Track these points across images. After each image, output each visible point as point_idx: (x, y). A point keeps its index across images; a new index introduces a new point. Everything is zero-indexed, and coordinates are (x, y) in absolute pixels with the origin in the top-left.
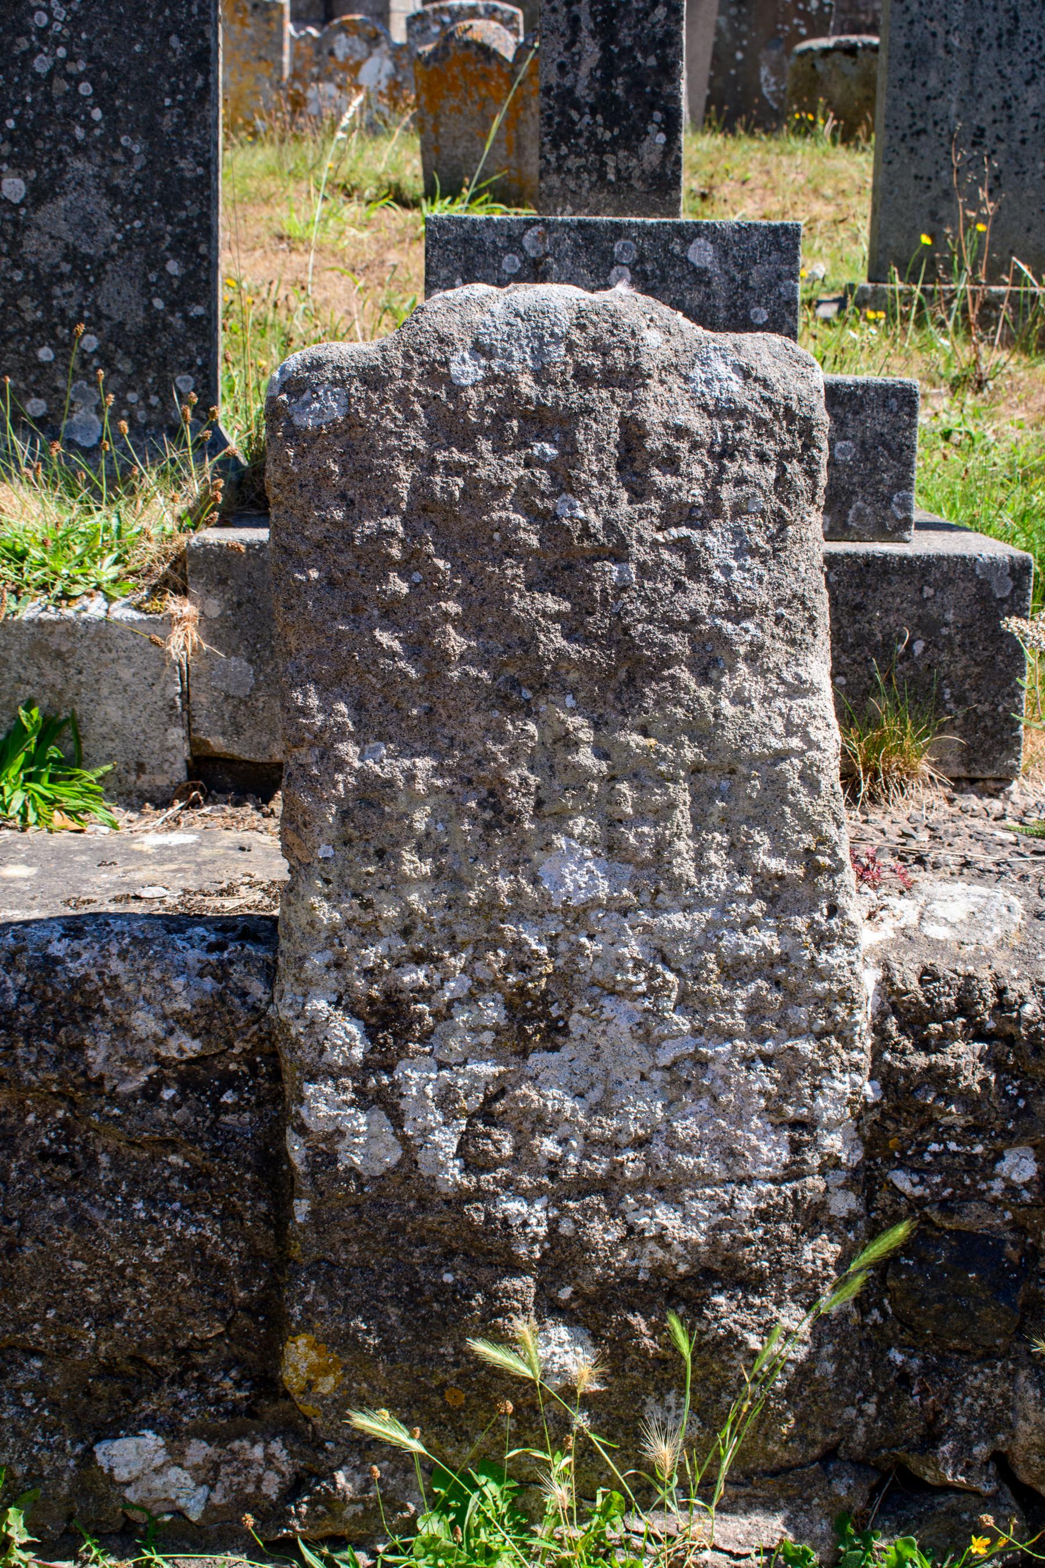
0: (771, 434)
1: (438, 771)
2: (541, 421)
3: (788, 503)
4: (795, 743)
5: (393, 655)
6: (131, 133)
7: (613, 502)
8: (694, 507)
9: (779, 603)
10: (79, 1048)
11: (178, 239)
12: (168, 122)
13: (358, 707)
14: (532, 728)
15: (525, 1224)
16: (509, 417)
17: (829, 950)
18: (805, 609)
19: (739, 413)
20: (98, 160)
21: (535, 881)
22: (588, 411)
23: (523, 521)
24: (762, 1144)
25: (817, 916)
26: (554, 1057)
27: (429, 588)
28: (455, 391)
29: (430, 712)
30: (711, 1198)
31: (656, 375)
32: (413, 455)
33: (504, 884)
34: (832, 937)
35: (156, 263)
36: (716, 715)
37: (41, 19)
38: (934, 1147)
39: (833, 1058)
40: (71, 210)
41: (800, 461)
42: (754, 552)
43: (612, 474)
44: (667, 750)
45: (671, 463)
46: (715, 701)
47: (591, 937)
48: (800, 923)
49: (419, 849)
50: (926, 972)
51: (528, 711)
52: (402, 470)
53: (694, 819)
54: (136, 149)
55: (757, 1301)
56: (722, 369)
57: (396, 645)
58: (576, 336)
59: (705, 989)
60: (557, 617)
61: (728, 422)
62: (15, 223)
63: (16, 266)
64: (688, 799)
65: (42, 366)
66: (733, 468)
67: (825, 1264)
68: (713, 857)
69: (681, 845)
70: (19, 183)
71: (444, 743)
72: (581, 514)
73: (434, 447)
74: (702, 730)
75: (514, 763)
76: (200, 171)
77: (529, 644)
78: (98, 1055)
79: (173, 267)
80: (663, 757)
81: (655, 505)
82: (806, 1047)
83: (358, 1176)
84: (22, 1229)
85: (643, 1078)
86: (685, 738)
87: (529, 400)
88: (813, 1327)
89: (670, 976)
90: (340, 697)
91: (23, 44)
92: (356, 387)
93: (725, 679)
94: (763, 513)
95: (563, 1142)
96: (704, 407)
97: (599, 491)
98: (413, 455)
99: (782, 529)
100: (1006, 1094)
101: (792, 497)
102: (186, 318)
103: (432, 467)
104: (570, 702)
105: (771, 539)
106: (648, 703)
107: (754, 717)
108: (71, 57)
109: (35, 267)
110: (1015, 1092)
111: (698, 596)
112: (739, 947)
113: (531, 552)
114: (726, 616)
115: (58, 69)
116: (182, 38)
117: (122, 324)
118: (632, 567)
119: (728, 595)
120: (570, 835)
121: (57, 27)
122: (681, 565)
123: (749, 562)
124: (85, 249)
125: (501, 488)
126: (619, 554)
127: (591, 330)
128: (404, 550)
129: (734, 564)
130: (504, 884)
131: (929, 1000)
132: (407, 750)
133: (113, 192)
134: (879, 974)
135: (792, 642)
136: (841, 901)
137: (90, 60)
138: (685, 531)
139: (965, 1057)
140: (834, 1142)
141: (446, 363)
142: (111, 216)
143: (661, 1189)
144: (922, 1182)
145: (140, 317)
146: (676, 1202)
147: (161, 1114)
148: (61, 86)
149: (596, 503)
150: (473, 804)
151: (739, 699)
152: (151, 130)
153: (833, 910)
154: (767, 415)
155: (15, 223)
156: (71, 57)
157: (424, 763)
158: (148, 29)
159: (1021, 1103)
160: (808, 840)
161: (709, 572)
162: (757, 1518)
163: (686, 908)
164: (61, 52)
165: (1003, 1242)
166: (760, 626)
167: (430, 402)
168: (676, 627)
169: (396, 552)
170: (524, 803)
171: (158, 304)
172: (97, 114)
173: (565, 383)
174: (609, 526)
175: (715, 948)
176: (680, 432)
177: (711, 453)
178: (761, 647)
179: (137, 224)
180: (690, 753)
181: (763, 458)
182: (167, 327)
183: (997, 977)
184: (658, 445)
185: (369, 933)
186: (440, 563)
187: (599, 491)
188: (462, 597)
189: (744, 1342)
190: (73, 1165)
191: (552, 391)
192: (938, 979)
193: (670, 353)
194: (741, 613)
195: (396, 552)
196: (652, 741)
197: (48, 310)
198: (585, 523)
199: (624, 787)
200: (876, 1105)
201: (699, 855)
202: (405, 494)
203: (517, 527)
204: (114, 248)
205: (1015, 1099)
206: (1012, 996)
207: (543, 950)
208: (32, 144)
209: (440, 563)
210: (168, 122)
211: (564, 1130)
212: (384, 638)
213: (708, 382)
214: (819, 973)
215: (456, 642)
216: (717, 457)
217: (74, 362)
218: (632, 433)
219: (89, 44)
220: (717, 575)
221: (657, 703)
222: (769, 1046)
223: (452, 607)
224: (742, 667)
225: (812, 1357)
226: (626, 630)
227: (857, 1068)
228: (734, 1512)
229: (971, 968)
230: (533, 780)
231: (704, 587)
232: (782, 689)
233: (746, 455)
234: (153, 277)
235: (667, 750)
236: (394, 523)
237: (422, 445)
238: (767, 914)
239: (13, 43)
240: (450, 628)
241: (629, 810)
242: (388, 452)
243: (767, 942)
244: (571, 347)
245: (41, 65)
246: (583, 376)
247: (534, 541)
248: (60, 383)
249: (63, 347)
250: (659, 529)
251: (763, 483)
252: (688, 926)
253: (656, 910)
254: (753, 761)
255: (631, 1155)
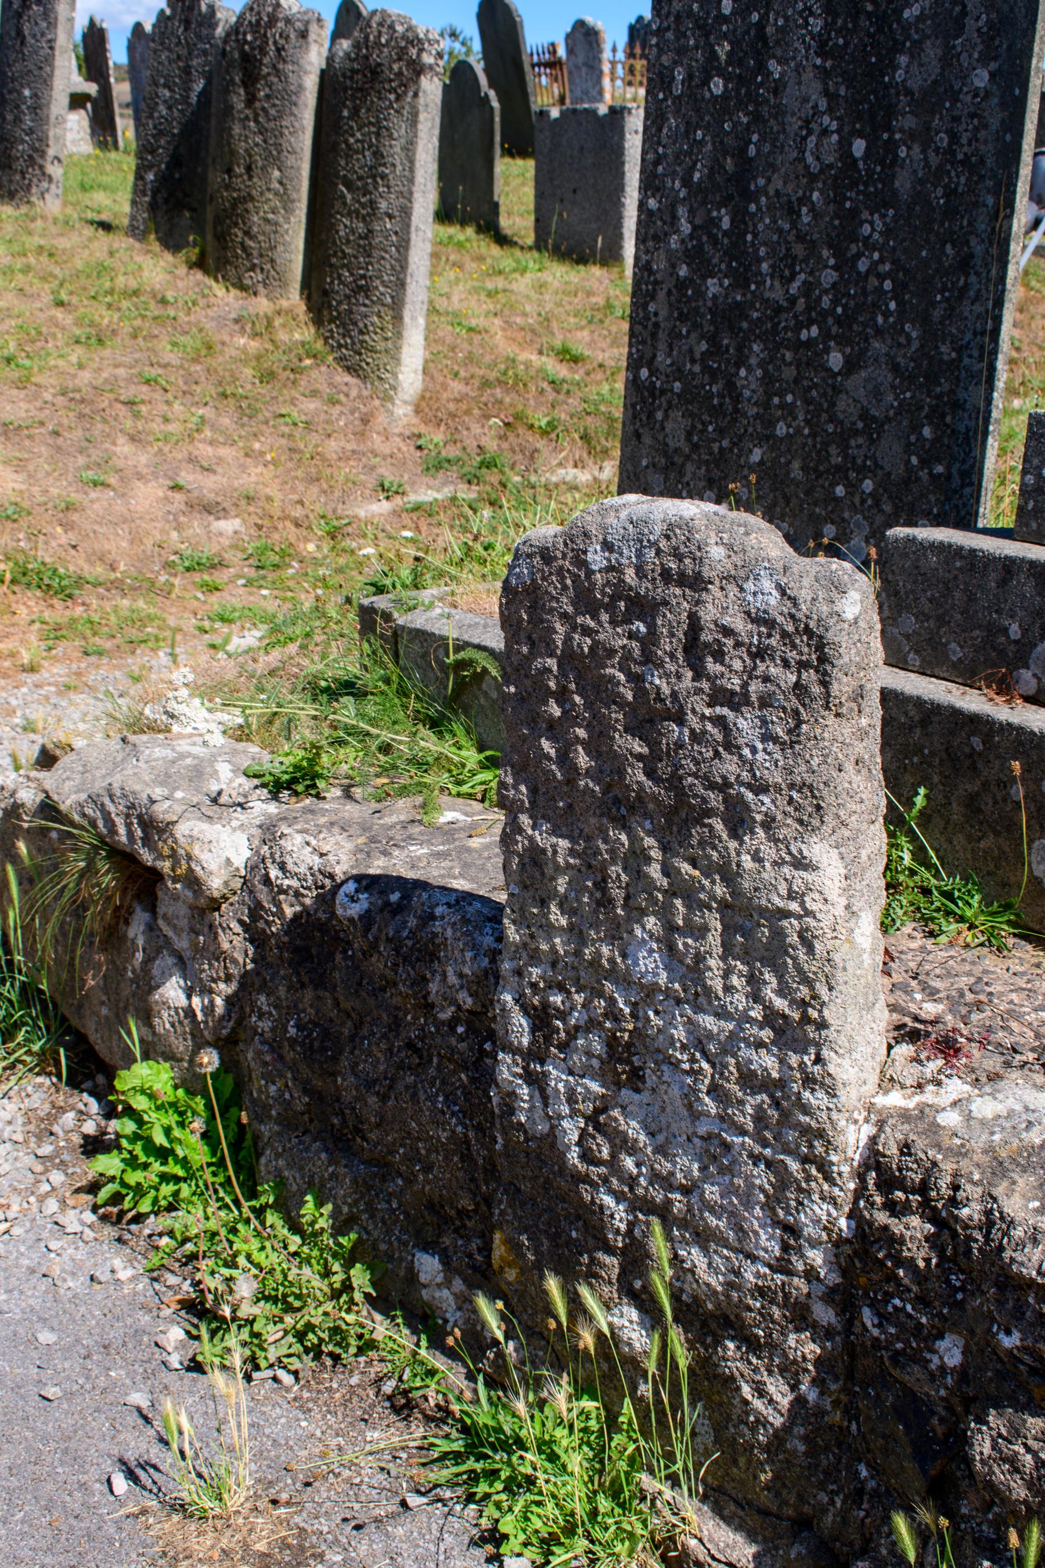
0: (794, 646)
1: (572, 852)
2: (643, 608)
3: (804, 705)
4: (794, 906)
5: (548, 757)
6: (913, 322)
7: (679, 677)
8: (733, 693)
9: (792, 786)
10: (424, 980)
11: (933, 409)
12: (937, 314)
13: (533, 791)
14: (623, 837)
15: (612, 1216)
16: (620, 599)
17: (813, 1090)
18: (814, 797)
19: (771, 624)
20: (889, 342)
21: (624, 956)
22: (665, 603)
23: (622, 677)
24: (761, 1232)
25: (806, 1058)
26: (636, 1097)
27: (569, 717)
28: (590, 573)
29: (570, 806)
30: (727, 1258)
31: (717, 582)
32: (564, 616)
33: (605, 950)
34: (815, 1081)
35: (916, 428)
36: (738, 865)
37: (866, 229)
38: (897, 1302)
39: (813, 1184)
40: (867, 380)
41: (817, 671)
42: (776, 740)
43: (680, 655)
44: (706, 883)
45: (719, 656)
46: (738, 854)
47: (657, 1013)
48: (794, 1059)
49: (560, 905)
50: (907, 1145)
51: (625, 827)
52: (558, 626)
53: (723, 945)
54: (914, 335)
55: (754, 1361)
56: (767, 585)
57: (552, 752)
58: (663, 544)
59: (727, 1085)
60: (640, 757)
61: (763, 629)
62: (834, 387)
63: (831, 420)
64: (719, 927)
65: (837, 500)
66: (761, 667)
67: (804, 1357)
68: (735, 981)
69: (712, 963)
70: (839, 355)
71: (577, 833)
72: (657, 682)
73: (578, 612)
74: (729, 875)
75: (613, 861)
76: (954, 355)
77: (621, 773)
78: (433, 987)
79: (927, 432)
80: (703, 888)
81: (705, 685)
82: (794, 1166)
83: (525, 1132)
84: (391, 1087)
85: (689, 1139)
86: (717, 877)
87: (631, 588)
88: (791, 1403)
89: (705, 1065)
90: (525, 782)
91: (854, 249)
92: (537, 560)
93: (746, 838)
94: (784, 709)
95: (638, 1165)
96: (748, 613)
97: (671, 667)
98: (564, 616)
99: (798, 726)
100: (948, 1282)
101: (807, 701)
102: (930, 474)
103: (574, 628)
104: (648, 825)
105: (790, 732)
106: (694, 842)
107: (765, 875)
108: (882, 260)
109: (842, 422)
110: (958, 1284)
111: (729, 767)
112: (751, 1062)
113: (629, 704)
114: (749, 786)
115: (872, 269)
116: (954, 246)
117: (889, 474)
118: (686, 732)
119: (751, 771)
120: (644, 928)
121: (876, 236)
122: (720, 738)
123: (771, 746)
124: (874, 412)
125: (611, 652)
126: (681, 721)
127: (674, 541)
128: (557, 684)
129: (760, 746)
130: (605, 950)
131: (900, 1170)
132: (555, 832)
133: (895, 368)
134: (873, 1131)
135: (801, 822)
136: (825, 1053)
137: (893, 263)
138: (725, 711)
139: (914, 1228)
140: (816, 1257)
141: (585, 552)
142: (893, 387)
143: (698, 1234)
144: (879, 1326)
145: (901, 469)
146: (705, 1250)
147: (453, 1041)
148: (873, 282)
149: (667, 675)
150: (589, 884)
151: (757, 858)
152: (925, 320)
153: (818, 1060)
154: (790, 628)
155: (834, 387)
156: (882, 260)
157: (564, 844)
158: (932, 238)
159: (960, 1296)
160: (804, 992)
161: (739, 748)
162: (739, 1538)
163: (717, 1015)
164: (876, 256)
165: (934, 1413)
166: (773, 802)
167: (576, 578)
168: (712, 786)
169: (552, 684)
170: (618, 894)
171: (914, 460)
172: (893, 305)
173: (654, 579)
174: (674, 694)
175: (734, 1055)
176: (727, 632)
177: (749, 653)
178: (774, 820)
179: (908, 395)
180: (720, 890)
181: (786, 664)
182: (918, 479)
183: (956, 1175)
184: (710, 638)
185: (535, 957)
186: (577, 699)
187: (671, 667)
188: (588, 728)
189: (739, 1388)
190: (421, 1057)
191: (646, 584)
192: (910, 1154)
193: (729, 566)
194: (760, 788)
195: (552, 684)
196: (697, 873)
197: (846, 457)
198: (658, 688)
199: (678, 902)
200: (848, 1241)
201: (727, 974)
202: (559, 644)
203: (619, 683)
204: (891, 413)
205: (956, 1290)
206: (961, 1195)
207: (627, 1010)
208: (850, 327)
209: (577, 699)
210: (937, 314)
211: (640, 1155)
212: (546, 745)
213: (755, 594)
214: (806, 1110)
215: (583, 760)
216: (753, 656)
217: (857, 500)
218: (695, 625)
219: (894, 249)
220: (746, 752)
221: (700, 843)
222: (768, 1152)
223: (581, 733)
224: (760, 833)
225: (787, 1429)
226: (681, 778)
227: (833, 1201)
228: (729, 1524)
229: (940, 1157)
230: (624, 877)
231: (735, 758)
232: (788, 858)
233: (773, 659)
234: (913, 438)
235: (706, 883)
236: (552, 663)
237: (570, 609)
238: (773, 1042)
239: (848, 248)
240: (580, 749)
241: (680, 923)
242: (552, 610)
243: (769, 1064)
244: (659, 552)
245: (863, 265)
246: (666, 575)
247: (630, 697)
248: (846, 515)
249: (852, 487)
250: (709, 705)
251: (782, 684)
252: (715, 1030)
253: (698, 1009)
254: (763, 911)
255: (679, 1197)
